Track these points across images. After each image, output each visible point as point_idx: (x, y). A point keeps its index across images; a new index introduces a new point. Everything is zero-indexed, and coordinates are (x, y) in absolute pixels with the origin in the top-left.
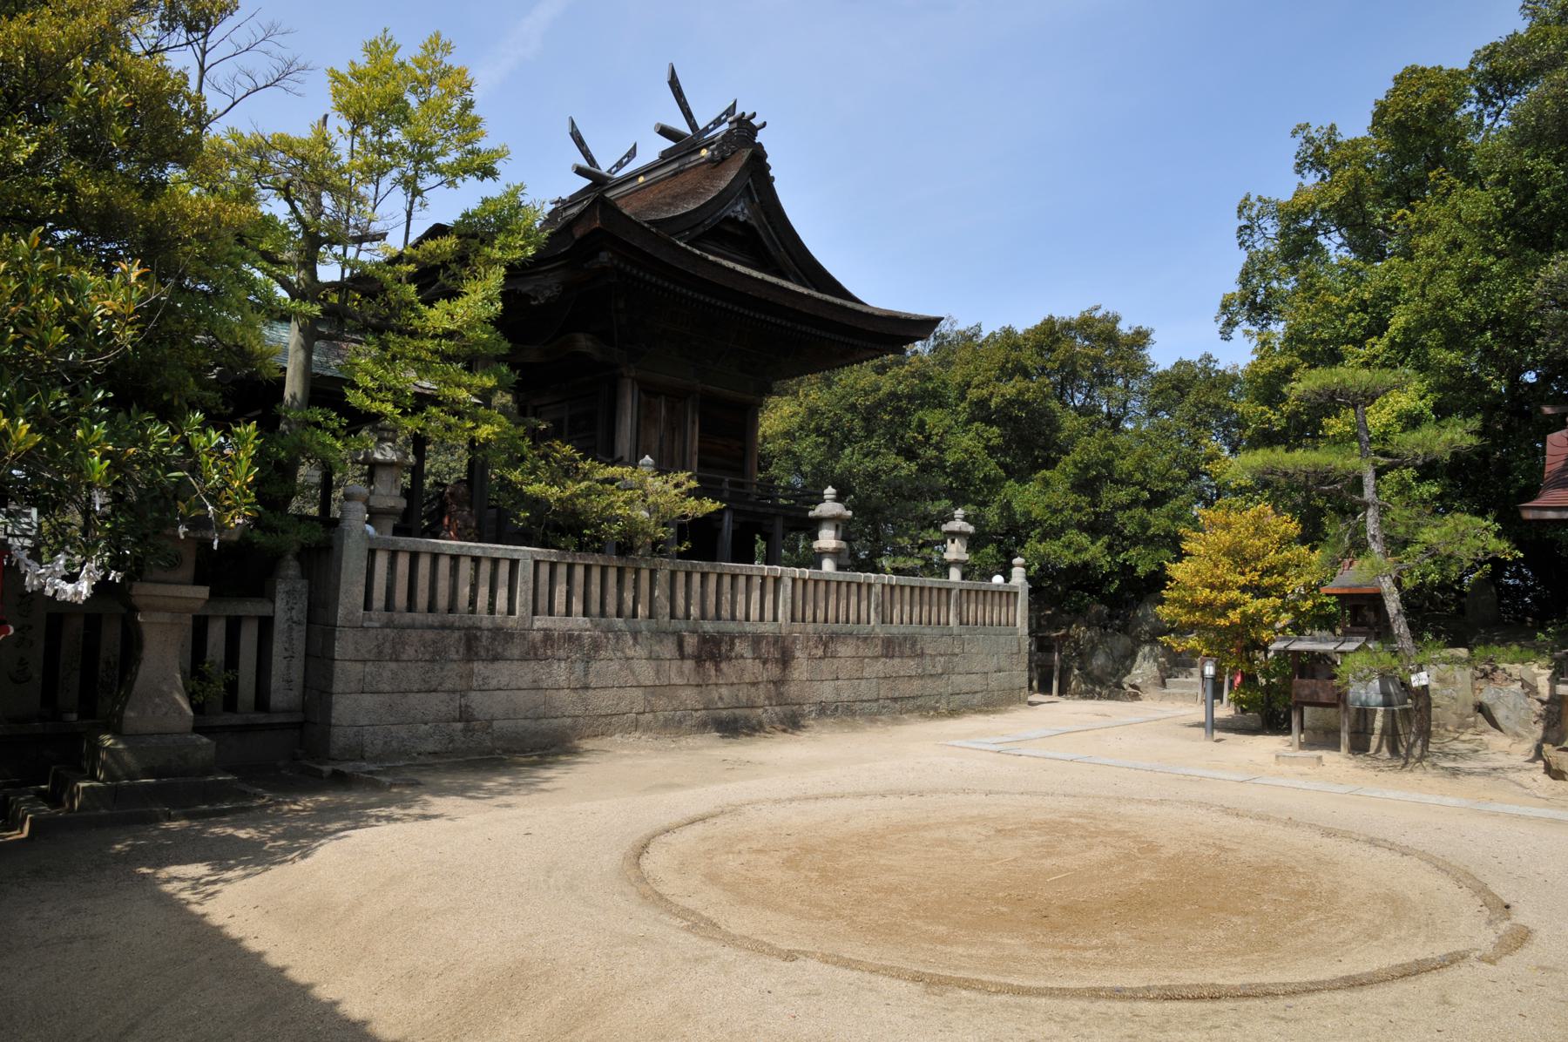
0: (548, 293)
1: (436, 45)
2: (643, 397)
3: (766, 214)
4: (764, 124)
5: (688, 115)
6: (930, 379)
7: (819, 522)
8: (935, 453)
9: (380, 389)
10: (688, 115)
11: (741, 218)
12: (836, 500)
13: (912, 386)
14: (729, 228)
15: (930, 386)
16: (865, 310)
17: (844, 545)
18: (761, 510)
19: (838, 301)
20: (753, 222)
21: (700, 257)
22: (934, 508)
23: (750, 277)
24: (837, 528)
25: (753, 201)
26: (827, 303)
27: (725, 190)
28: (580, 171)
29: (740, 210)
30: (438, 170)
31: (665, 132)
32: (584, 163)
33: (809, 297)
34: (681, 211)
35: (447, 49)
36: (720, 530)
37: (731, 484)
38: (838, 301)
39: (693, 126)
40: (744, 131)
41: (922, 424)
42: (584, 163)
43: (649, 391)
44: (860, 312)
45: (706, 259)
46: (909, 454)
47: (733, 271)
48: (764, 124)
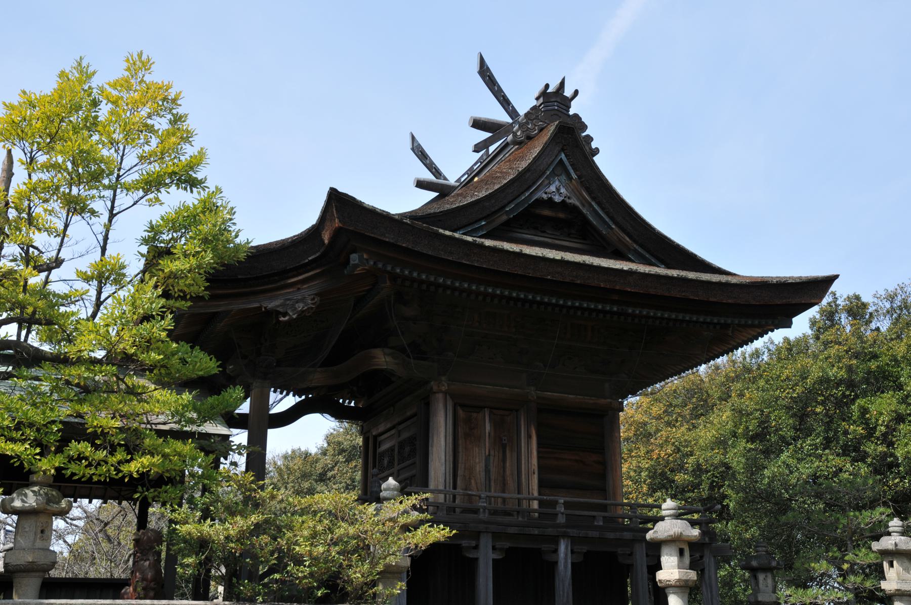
0: (300, 306)
1: (139, 64)
2: (461, 413)
3: (588, 190)
4: (576, 93)
5: (505, 102)
6: (875, 356)
7: (656, 548)
8: (881, 449)
9: (18, 428)
10: (505, 102)
11: (557, 199)
12: (677, 516)
13: (850, 369)
14: (547, 212)
15: (873, 365)
16: (734, 280)
17: (692, 575)
18: (611, 535)
19: (691, 275)
20: (573, 201)
21: (473, 244)
22: (867, 518)
23: (544, 259)
24: (681, 553)
25: (570, 178)
26: (658, 277)
27: (527, 169)
28: (421, 185)
29: (556, 190)
30: (128, 188)
31: (478, 124)
32: (428, 176)
33: (630, 273)
34: (470, 200)
35: (146, 65)
36: (556, 563)
37: (567, 505)
38: (691, 275)
39: (513, 113)
40: (555, 101)
41: (864, 411)
42: (428, 176)
43: (466, 409)
44: (727, 285)
45: (482, 246)
46: (853, 450)
47: (520, 255)
48: (576, 93)
